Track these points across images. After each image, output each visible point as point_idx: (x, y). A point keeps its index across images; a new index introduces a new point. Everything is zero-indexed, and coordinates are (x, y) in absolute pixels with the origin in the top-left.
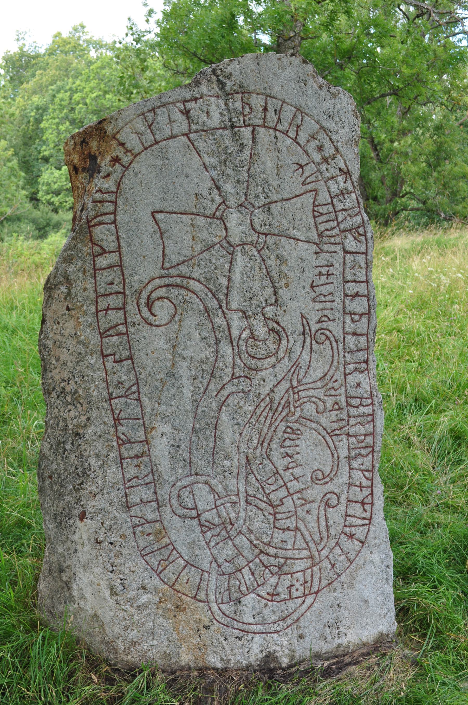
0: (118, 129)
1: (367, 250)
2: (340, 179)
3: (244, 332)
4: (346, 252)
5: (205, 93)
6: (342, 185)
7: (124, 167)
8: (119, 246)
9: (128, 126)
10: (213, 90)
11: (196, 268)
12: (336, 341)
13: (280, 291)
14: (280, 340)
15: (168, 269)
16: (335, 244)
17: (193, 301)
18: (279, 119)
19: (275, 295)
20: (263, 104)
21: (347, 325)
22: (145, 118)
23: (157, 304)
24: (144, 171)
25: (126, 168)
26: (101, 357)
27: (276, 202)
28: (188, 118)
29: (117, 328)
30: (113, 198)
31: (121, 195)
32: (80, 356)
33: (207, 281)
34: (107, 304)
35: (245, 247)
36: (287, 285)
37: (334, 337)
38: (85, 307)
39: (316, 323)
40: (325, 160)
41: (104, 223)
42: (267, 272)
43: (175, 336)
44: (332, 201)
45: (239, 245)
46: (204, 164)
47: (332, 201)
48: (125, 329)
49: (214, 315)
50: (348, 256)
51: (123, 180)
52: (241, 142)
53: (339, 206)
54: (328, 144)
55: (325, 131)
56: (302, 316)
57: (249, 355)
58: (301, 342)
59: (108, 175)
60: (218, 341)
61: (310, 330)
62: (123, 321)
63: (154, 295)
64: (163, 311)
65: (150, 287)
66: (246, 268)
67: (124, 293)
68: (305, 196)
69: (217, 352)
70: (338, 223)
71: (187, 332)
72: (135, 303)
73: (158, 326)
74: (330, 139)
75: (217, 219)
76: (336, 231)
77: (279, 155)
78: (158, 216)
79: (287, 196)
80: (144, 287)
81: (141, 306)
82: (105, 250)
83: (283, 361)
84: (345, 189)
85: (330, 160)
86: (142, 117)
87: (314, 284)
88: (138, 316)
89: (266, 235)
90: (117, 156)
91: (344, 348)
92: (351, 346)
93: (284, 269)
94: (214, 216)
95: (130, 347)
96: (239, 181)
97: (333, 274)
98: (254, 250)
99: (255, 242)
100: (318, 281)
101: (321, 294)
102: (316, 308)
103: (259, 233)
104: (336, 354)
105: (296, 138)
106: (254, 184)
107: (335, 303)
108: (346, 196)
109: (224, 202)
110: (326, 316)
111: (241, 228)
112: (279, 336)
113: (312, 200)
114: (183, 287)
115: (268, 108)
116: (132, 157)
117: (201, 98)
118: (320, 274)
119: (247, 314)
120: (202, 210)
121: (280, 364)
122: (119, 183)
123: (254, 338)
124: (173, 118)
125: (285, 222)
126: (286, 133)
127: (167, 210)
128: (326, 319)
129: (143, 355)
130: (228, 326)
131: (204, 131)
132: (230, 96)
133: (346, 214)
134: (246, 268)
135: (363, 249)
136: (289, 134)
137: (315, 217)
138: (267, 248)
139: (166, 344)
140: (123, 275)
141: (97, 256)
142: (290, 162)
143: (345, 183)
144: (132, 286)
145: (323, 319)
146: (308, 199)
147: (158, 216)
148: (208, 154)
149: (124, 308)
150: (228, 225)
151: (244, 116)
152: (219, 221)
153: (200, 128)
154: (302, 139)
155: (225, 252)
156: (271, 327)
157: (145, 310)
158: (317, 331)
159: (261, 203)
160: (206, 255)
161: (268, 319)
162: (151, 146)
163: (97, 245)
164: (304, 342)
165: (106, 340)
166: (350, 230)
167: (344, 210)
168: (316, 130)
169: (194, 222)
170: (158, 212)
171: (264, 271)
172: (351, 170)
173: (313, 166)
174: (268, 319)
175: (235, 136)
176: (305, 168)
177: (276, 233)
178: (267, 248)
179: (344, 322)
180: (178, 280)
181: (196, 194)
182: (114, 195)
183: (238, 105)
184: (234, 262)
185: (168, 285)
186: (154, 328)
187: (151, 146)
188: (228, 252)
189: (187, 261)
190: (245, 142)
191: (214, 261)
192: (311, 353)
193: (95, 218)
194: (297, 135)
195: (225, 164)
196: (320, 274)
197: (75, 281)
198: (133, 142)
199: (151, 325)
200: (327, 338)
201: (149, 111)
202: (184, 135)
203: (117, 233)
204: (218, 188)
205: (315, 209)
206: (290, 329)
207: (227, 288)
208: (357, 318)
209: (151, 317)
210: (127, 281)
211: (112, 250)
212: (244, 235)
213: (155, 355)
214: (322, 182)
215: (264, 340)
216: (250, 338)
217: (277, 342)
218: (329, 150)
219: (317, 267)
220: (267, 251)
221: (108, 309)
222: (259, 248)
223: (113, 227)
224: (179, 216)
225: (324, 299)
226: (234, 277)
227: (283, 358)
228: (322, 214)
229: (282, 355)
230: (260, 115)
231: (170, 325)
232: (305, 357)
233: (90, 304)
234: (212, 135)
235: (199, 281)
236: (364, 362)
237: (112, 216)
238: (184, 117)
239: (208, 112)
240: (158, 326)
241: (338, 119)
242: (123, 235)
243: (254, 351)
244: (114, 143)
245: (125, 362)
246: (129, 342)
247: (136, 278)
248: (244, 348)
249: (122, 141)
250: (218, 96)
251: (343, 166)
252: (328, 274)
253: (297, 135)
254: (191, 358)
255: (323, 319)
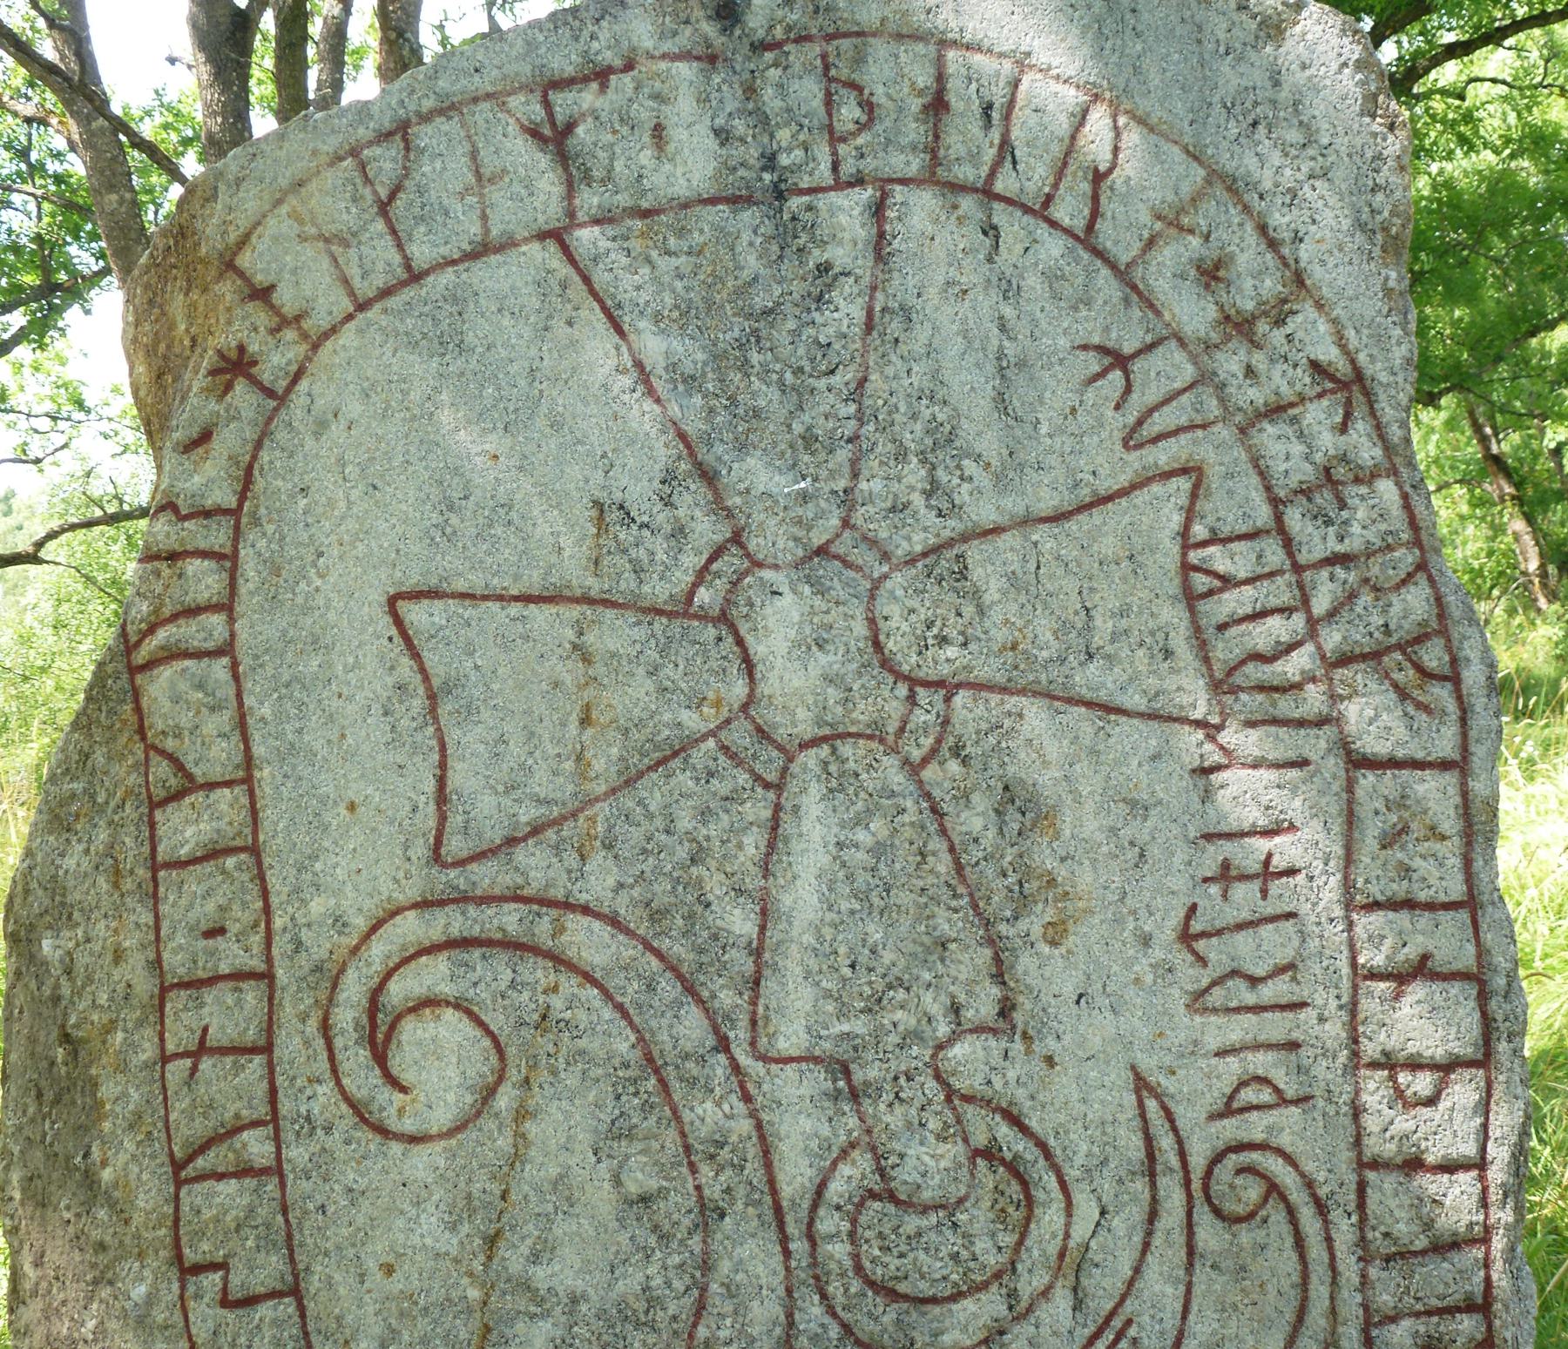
0: (244, 224)
1: (1465, 749)
2: (1319, 416)
3: (845, 1170)
4: (1359, 762)
5: (648, 44)
6: (1327, 442)
7: (270, 393)
8: (249, 761)
9: (284, 209)
10: (688, 31)
11: (598, 859)
12: (1321, 1208)
13: (1025, 963)
14: (1030, 1201)
15: (461, 863)
16: (1301, 723)
17: (582, 1017)
18: (1006, 146)
19: (999, 977)
20: (924, 79)
21: (1371, 1123)
22: (363, 167)
23: (412, 1031)
24: (354, 408)
25: (278, 397)
26: (174, 1274)
27: (997, 530)
28: (563, 158)
29: (237, 1141)
30: (217, 536)
31: (256, 522)
32: (103, 1259)
33: (642, 927)
34: (197, 1026)
35: (846, 749)
36: (1056, 934)
37: (1309, 1184)
38: (120, 1036)
39: (1214, 1117)
40: (1239, 326)
41: (187, 655)
42: (959, 868)
43: (496, 1188)
44: (1279, 518)
45: (815, 742)
46: (639, 365)
47: (1279, 518)
48: (270, 1148)
49: (692, 1082)
50: (1367, 781)
51: (265, 456)
52: (816, 256)
53: (1315, 542)
54: (1248, 254)
55: (1232, 190)
56: (1141, 1084)
57: (871, 1284)
58: (1136, 1213)
59: (205, 437)
60: (708, 1214)
61: (1183, 1155)
62: (263, 1111)
63: (399, 990)
64: (439, 1062)
65: (379, 951)
66: (846, 855)
67: (268, 976)
68: (1140, 497)
69: (706, 1266)
70: (1313, 623)
71: (554, 1171)
72: (312, 1026)
73: (414, 1139)
74: (1262, 229)
75: (703, 617)
76: (1299, 662)
77: (1008, 311)
78: (416, 614)
79: (1048, 502)
80: (355, 951)
81: (339, 1042)
82: (190, 777)
83: (1043, 1312)
84: (1344, 458)
85: (1262, 327)
86: (348, 162)
87: (1196, 926)
88: (326, 1090)
89: (946, 688)
90: (241, 349)
91: (1363, 1242)
92: (1401, 1229)
93: (1044, 857)
94: (683, 608)
95: (289, 1236)
96: (809, 439)
97: (1291, 872)
98: (890, 762)
99: (892, 728)
100: (1214, 909)
101: (1234, 973)
102: (1213, 1042)
103: (913, 682)
104: (1319, 1272)
105: (1090, 228)
106: (884, 447)
107: (1307, 1015)
108: (1352, 492)
109: (737, 538)
110: (1264, 1081)
111: (823, 659)
112: (1025, 1184)
113: (1177, 519)
114: (535, 950)
115: (952, 98)
116: (303, 348)
117: (629, 66)
118: (1226, 875)
119: (858, 1076)
120: (628, 582)
121: (1026, 1329)
122: (249, 469)
123: (892, 1197)
124: (490, 164)
125: (1044, 627)
126: (1041, 210)
127: (460, 585)
128: (1266, 1096)
129: (344, 1284)
130: (762, 1138)
131: (645, 214)
132: (769, 56)
133: (1352, 577)
134: (846, 855)
135: (1445, 743)
136: (1061, 213)
137: (1191, 598)
138: (956, 751)
139: (453, 1227)
140: (265, 894)
141: (163, 803)
142: (1063, 342)
143: (1343, 428)
144: (299, 945)
145: (1248, 1095)
146: (1163, 509)
147: (416, 614)
148: (657, 318)
149: (267, 1049)
150: (758, 649)
151: (835, 139)
152: (711, 632)
153: (624, 200)
154: (1119, 238)
155: (743, 778)
156: (980, 1139)
157: (356, 1059)
158: (1218, 1158)
159: (919, 542)
160: (654, 793)
161: (968, 1099)
162: (386, 293)
163: (162, 752)
164: (1153, 1216)
165: (192, 1196)
166: (1376, 655)
167: (1343, 559)
168: (1186, 189)
169: (590, 638)
170: (416, 595)
171: (942, 865)
172: (1369, 371)
173: (1179, 356)
174: (968, 1099)
175: (789, 237)
176: (1137, 366)
177: (1000, 678)
178: (956, 751)
179: (1357, 1111)
180: (510, 919)
181: (598, 504)
182: (227, 523)
183: (809, 91)
184: (788, 826)
185: (465, 943)
186: (396, 1148)
187: (386, 293)
188: (758, 778)
189: (557, 822)
190: (839, 256)
191: (685, 822)
192: (1190, 1267)
193: (152, 630)
194: (1095, 213)
195: (744, 366)
196: (1226, 875)
197: (87, 914)
198: (310, 285)
199: (383, 1131)
200: (1273, 1189)
201: (384, 137)
202: (542, 236)
203: (239, 695)
204: (708, 476)
205: (1194, 557)
206: (1079, 1150)
207: (757, 952)
208: (1422, 1083)
209: (385, 1095)
210: (278, 923)
211: (217, 773)
212: (833, 694)
213: (396, 1284)
214: (1223, 432)
215: (949, 1207)
216: (873, 1195)
217: (1016, 1215)
218: (1254, 282)
219: (1209, 837)
220: (954, 766)
221: (202, 1049)
222: (916, 755)
223: (219, 669)
224: (515, 609)
225: (1250, 998)
226: (787, 900)
227: (1046, 1293)
228: (1227, 582)
229: (1040, 1280)
230: (914, 131)
231: (471, 1134)
232: (1160, 1285)
233: (140, 1023)
234: (681, 232)
235: (614, 921)
236: (1469, 1307)
237: (216, 621)
238: (543, 160)
239: (658, 131)
240: (414, 1139)
241: (1294, 136)
242: (261, 708)
243: (894, 1263)
244: (227, 289)
245: (265, 1311)
246: (285, 1210)
247: (317, 906)
248: (839, 1251)
249: (260, 279)
250: (712, 59)
251: (1328, 353)
252: (1267, 873)
253: (1095, 213)
254: (575, 1300)
255: (1248, 1095)
